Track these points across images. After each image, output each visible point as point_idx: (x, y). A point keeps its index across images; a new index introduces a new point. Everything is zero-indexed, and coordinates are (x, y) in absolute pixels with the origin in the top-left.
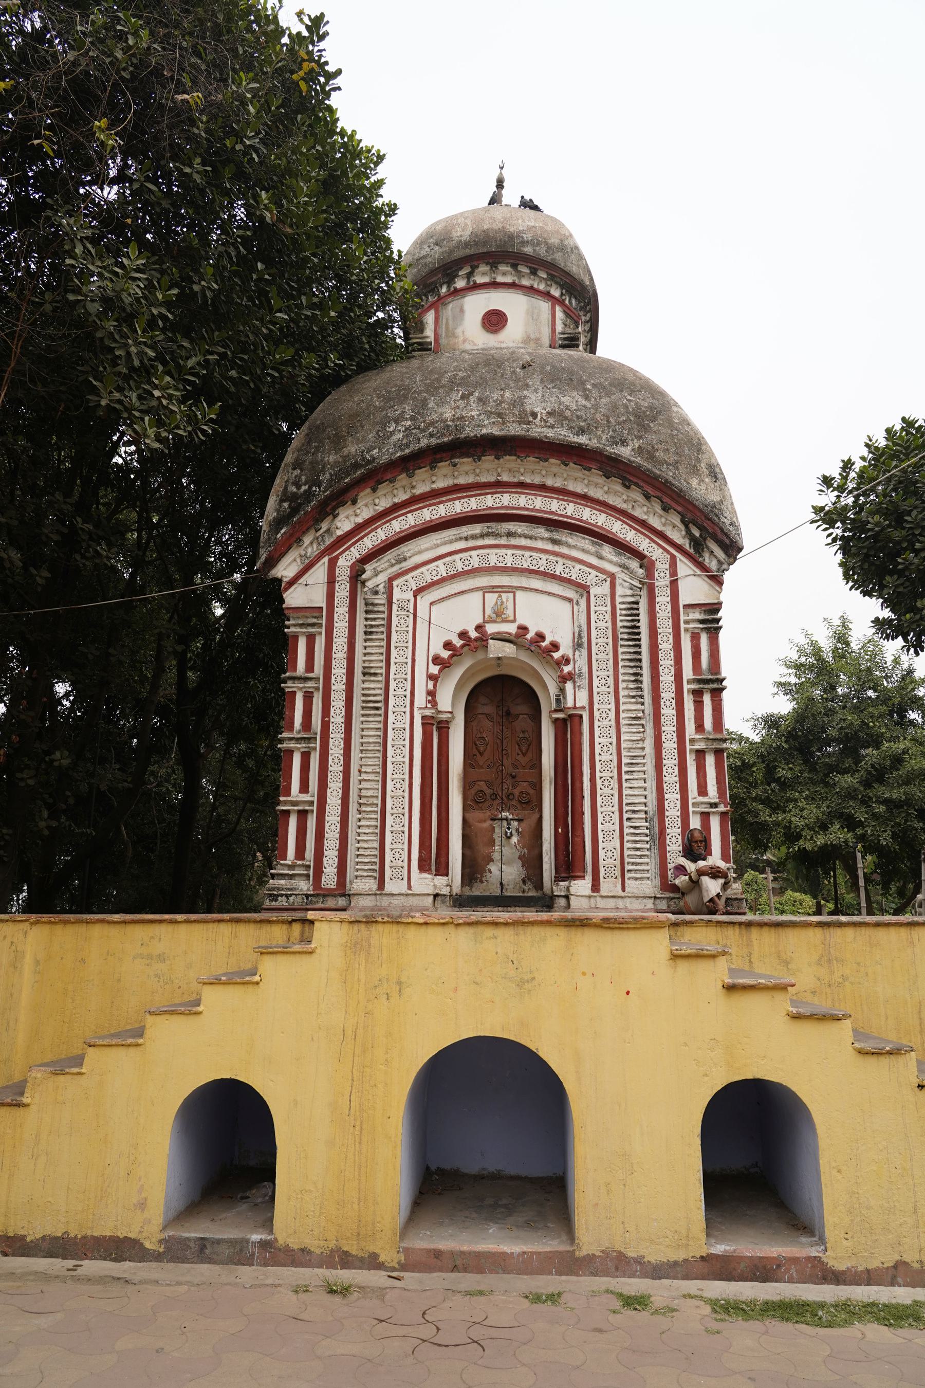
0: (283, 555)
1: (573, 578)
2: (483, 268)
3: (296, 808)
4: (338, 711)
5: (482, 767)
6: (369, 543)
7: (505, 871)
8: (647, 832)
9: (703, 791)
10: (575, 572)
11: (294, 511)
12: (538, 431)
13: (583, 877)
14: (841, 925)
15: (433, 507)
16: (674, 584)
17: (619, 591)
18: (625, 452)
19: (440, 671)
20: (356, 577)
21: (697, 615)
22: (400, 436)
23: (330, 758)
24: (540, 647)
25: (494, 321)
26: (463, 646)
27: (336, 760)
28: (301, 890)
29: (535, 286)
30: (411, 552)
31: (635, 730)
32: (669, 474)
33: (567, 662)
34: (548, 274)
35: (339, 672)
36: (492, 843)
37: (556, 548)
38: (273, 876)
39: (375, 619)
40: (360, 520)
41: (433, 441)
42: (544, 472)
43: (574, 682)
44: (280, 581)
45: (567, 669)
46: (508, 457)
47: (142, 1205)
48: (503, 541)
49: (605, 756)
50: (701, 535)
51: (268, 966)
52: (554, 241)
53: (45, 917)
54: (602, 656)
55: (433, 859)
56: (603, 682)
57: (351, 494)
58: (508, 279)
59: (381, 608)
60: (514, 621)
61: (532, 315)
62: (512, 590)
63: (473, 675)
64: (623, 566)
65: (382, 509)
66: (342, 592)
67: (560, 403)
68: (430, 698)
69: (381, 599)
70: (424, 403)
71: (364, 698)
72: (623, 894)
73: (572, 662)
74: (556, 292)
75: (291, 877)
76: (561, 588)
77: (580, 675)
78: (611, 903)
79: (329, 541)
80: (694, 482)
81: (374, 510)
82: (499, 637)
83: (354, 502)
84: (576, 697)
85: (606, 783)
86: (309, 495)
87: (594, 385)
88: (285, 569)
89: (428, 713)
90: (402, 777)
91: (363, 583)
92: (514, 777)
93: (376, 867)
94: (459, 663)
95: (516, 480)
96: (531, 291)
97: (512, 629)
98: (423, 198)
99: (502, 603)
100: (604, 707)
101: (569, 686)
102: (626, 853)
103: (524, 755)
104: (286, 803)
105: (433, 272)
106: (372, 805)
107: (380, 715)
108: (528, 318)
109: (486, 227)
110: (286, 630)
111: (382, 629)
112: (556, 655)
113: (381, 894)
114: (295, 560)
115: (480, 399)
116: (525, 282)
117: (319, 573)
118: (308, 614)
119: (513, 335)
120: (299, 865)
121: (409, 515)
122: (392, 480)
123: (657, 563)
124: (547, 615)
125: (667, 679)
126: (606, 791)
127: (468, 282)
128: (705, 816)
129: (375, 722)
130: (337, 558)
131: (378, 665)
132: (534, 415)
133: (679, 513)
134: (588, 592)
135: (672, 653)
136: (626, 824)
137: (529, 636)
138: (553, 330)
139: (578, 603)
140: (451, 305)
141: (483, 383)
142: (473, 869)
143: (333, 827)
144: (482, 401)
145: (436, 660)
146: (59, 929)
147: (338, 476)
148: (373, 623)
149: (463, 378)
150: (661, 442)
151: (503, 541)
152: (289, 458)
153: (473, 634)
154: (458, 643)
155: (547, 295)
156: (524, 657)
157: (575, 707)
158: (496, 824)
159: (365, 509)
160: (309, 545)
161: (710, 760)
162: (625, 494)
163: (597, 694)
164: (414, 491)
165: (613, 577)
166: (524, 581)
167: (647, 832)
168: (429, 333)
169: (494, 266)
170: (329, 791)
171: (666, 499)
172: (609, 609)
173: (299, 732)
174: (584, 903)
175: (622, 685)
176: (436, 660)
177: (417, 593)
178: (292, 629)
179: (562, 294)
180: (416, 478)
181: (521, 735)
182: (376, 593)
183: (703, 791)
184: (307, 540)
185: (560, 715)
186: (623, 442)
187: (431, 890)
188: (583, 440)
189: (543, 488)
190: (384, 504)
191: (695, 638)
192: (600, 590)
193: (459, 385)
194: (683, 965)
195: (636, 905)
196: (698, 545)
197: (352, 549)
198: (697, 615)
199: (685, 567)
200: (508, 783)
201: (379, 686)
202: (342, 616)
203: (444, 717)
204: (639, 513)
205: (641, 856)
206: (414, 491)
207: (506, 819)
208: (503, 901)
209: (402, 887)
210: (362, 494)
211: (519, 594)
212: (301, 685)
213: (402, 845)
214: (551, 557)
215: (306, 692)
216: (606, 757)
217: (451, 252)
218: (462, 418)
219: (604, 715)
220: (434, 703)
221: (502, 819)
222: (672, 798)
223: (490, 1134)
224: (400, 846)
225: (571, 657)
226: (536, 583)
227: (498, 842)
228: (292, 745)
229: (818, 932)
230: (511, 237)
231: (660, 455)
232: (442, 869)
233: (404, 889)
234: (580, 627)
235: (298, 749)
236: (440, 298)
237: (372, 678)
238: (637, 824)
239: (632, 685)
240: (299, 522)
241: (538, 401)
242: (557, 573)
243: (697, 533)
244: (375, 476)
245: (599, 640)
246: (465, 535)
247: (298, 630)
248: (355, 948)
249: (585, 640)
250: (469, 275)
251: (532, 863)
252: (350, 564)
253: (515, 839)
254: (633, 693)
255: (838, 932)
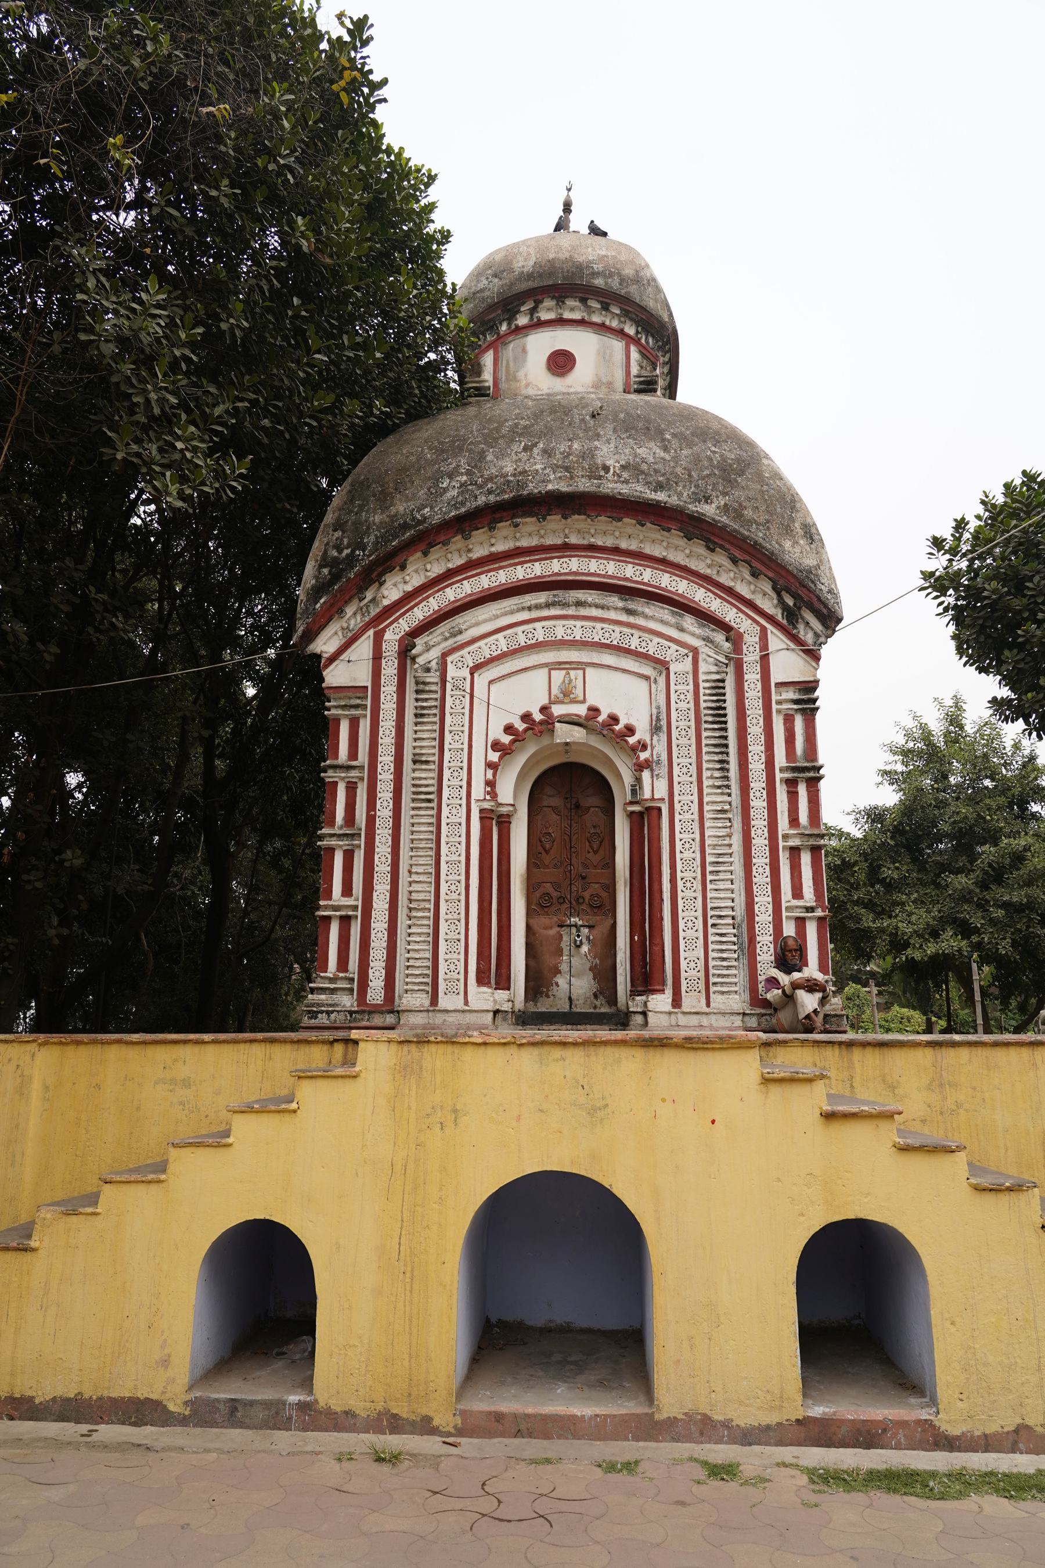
0: (322, 627)
1: (651, 653)
2: (548, 303)
3: (338, 913)
4: (385, 804)
5: (547, 867)
6: (420, 613)
7: (574, 984)
8: (735, 939)
9: (797, 894)
10: (653, 646)
11: (335, 577)
12: (610, 486)
13: (662, 991)
14: (954, 1044)
15: (492, 573)
16: (765, 659)
17: (703, 667)
18: (709, 510)
19: (501, 758)
20: (405, 652)
21: (791, 694)
22: (455, 493)
23: (376, 857)
24: (613, 731)
25: (561, 362)
26: (526, 730)
27: (383, 859)
28: (344, 1006)
29: (607, 323)
30: (467, 624)
31: (720, 825)
32: (758, 535)
33: (644, 747)
34: (621, 309)
35: (386, 759)
36: (559, 952)
37: (631, 619)
38: (312, 991)
39: (426, 700)
40: (409, 588)
41: (492, 498)
42: (617, 533)
43: (652, 771)
44: (318, 657)
45: (643, 756)
46: (576, 516)
47: (165, 1363)
48: (571, 611)
49: (687, 854)
50: (795, 604)
51: (306, 1091)
52: (628, 272)
53: (55, 1037)
54: (683, 741)
55: (493, 971)
56: (685, 770)
57: (399, 559)
58: (577, 316)
59: (433, 688)
60: (584, 701)
61: (604, 356)
62: (582, 666)
63: (538, 763)
64: (707, 639)
65: (435, 575)
66: (389, 669)
67: (636, 455)
68: (489, 789)
69: (433, 677)
70: (482, 455)
71: (414, 789)
72: (707, 1010)
73: (649, 748)
74: (630, 330)
75: (333, 991)
76: (637, 664)
77: (658, 762)
78: (694, 1020)
79: (374, 611)
80: (787, 544)
81: (426, 577)
82: (566, 719)
83: (403, 568)
84: (654, 788)
85: (688, 885)
86: (351, 560)
87: (674, 435)
88: (325, 644)
89: (487, 805)
90: (458, 878)
91: (413, 659)
92: (584, 878)
93: (429, 980)
94: (522, 749)
95: (585, 542)
96: (602, 328)
97: (581, 710)
98: (480, 223)
99: (570, 681)
100: (686, 799)
101: (646, 775)
102: (711, 963)
103: (596, 852)
104: (326, 907)
105: (491, 308)
106: (424, 909)
107: (433, 808)
108: (599, 360)
109: (551, 256)
110: (326, 713)
111: (434, 711)
112: (632, 740)
113: (434, 1011)
114: (336, 633)
115: (545, 451)
116: (596, 319)
117: (364, 648)
118: (350, 694)
119: (581, 379)
120: (342, 978)
121: (465, 582)
122: (445, 543)
123: (746, 635)
124: (621, 695)
125: (757, 765)
126: (688, 893)
127: (532, 319)
128: (800, 922)
129: (426, 817)
130: (384, 630)
131: (430, 751)
132: (606, 469)
133: (769, 579)
134: (668, 669)
135: (763, 737)
136: (711, 930)
137: (600, 719)
138: (628, 373)
139: (656, 681)
140: (512, 345)
141: (548, 432)
142: (538, 982)
143: (380, 935)
144: (547, 453)
145: (496, 746)
146: (70, 1050)
147: (385, 539)
148: (425, 704)
149: (525, 427)
150: (749, 499)
151: (571, 611)
152: (329, 518)
153: (538, 717)
154: (520, 726)
155: (621, 333)
156: (595, 742)
157: (653, 799)
158: (564, 932)
159: (415, 575)
160: (352, 616)
161: (806, 859)
162: (710, 557)
163: (677, 785)
164: (470, 555)
165: (695, 651)
166: (595, 657)
167: (735, 939)
168: (487, 376)
169: (560, 300)
170: (375, 894)
171: (755, 564)
172: (691, 687)
173: (341, 828)
174: (664, 1020)
175: (706, 774)
176: (496, 746)
177: (473, 671)
178: (333, 711)
179: (637, 332)
180: (473, 540)
181: (592, 831)
182: (428, 670)
183: (797, 894)
184: (350, 610)
185: (636, 808)
186: (707, 499)
187: (490, 1006)
188: (661, 496)
189: (616, 551)
190: (436, 569)
191: (789, 720)
192: (681, 667)
193: (521, 435)
194: (775, 1090)
195: (723, 1022)
196: (792, 615)
197: (401, 620)
198: (791, 694)
199: (777, 641)
200: (577, 886)
201: (431, 775)
202: (389, 697)
203: (504, 810)
204: (724, 579)
205: (728, 968)
206: (470, 555)
207: (576, 926)
208: (572, 1019)
209: (458, 1002)
210: (411, 559)
211: (589, 671)
212: (343, 775)
213: (459, 953)
214: (625, 630)
215: (348, 782)
216: (687, 855)
217: (512, 284)
218: (524, 472)
219: (686, 808)
220: (493, 795)
221: (570, 926)
222: (763, 901)
223: (558, 1281)
224: (455, 956)
225: (649, 742)
226: (609, 659)
227: (566, 951)
228: (333, 842)
229: (929, 1052)
230: (580, 268)
231: (748, 513)
232: (504, 982)
233: (460, 1004)
234: (658, 708)
235: (340, 846)
236: (500, 337)
237: (424, 767)
238: (724, 931)
239: (717, 774)
240: (340, 590)
241: (610, 453)
242: (633, 647)
243: (790, 602)
244: (427, 538)
245: (680, 723)
246: (528, 604)
247: (340, 712)
248: (404, 1071)
249: (664, 723)
250: (533, 311)
251: (605, 975)
252: (398, 637)
253: (585, 948)
254: (718, 783)
255: (951, 1052)
